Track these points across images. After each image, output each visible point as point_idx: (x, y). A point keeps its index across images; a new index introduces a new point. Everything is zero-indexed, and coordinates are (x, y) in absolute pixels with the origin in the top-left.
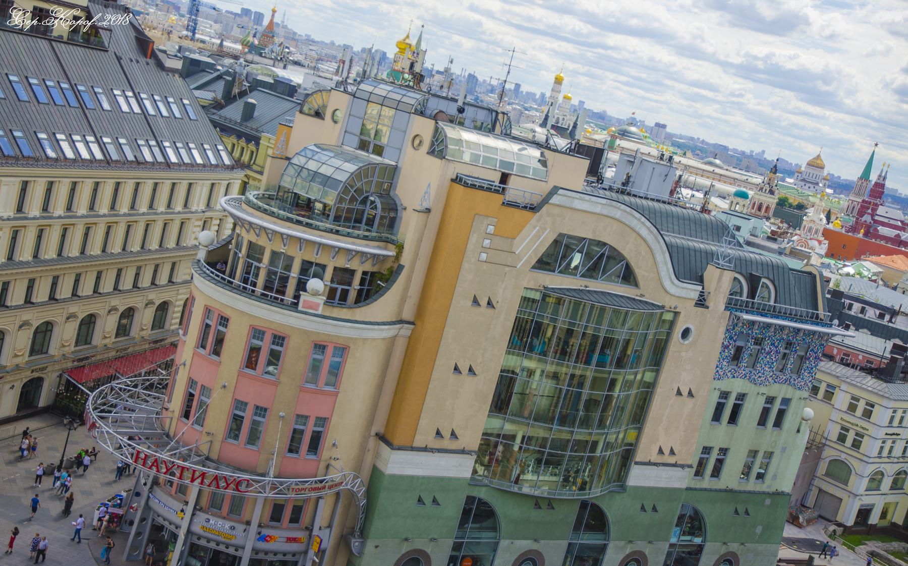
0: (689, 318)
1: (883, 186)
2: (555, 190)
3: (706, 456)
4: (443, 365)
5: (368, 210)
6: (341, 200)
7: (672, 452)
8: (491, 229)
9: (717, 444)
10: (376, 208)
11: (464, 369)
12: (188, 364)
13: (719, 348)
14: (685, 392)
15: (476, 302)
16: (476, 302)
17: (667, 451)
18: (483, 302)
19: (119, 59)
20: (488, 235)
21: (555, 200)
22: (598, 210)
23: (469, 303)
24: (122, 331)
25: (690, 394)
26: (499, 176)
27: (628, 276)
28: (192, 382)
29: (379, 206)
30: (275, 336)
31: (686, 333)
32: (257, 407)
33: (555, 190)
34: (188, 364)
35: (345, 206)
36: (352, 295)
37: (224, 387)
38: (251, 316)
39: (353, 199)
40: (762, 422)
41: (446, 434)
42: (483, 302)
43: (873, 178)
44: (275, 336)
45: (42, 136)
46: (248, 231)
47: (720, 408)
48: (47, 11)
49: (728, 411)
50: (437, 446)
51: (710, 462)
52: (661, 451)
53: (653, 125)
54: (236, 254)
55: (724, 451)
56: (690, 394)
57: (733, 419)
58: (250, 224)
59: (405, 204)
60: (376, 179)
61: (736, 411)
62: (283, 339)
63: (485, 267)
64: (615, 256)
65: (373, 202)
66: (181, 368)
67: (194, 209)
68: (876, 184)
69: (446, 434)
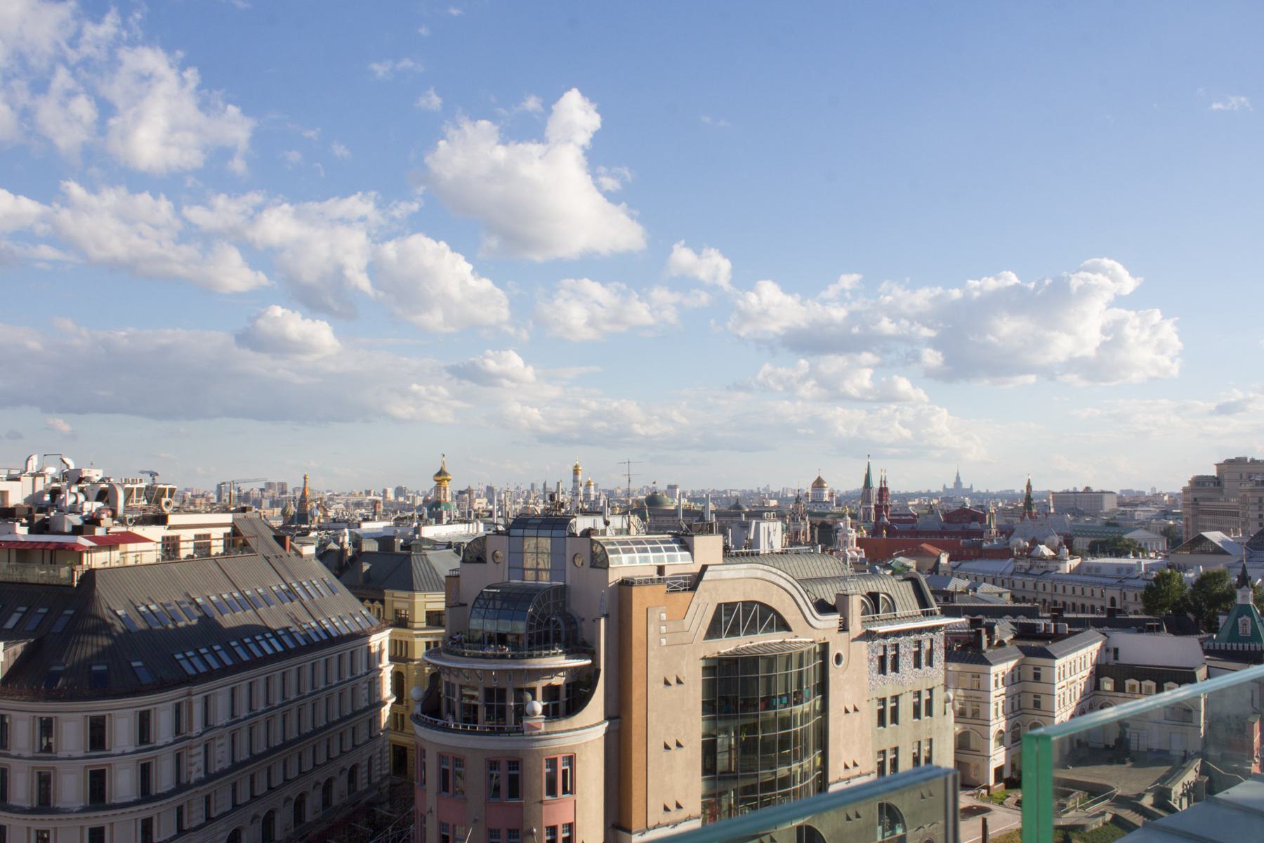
0: (838, 645)
1: (886, 489)
2: (704, 568)
3: (515, 772)
4: (655, 745)
5: (552, 629)
6: (530, 627)
7: (855, 765)
8: (664, 616)
9: (887, 746)
10: (558, 626)
11: (672, 745)
12: (434, 809)
13: (866, 662)
14: (851, 709)
15: (667, 683)
16: (667, 683)
17: (850, 765)
18: (673, 681)
19: (267, 559)
20: (661, 622)
21: (707, 576)
22: (742, 574)
23: (662, 685)
24: (326, 802)
25: (856, 710)
26: (655, 570)
27: (784, 626)
28: (443, 826)
29: (561, 623)
30: (510, 762)
31: (838, 658)
32: (510, 831)
33: (704, 568)
34: (434, 809)
35: (534, 631)
36: (562, 707)
37: (475, 821)
38: (484, 751)
39: (539, 624)
40: (917, 714)
41: (672, 807)
42: (673, 681)
43: (876, 485)
44: (510, 762)
45: (233, 644)
46: (457, 677)
47: (881, 714)
48: (178, 537)
49: (887, 714)
50: (667, 821)
51: (887, 763)
52: (846, 767)
53: (665, 488)
54: (449, 701)
55: (896, 750)
56: (856, 710)
57: (895, 719)
58: (460, 669)
59: (583, 616)
60: (552, 601)
61: (895, 711)
62: (517, 763)
63: (666, 650)
64: (766, 609)
65: (555, 622)
66: (428, 818)
67: (359, 673)
68: (881, 489)
69: (672, 807)
